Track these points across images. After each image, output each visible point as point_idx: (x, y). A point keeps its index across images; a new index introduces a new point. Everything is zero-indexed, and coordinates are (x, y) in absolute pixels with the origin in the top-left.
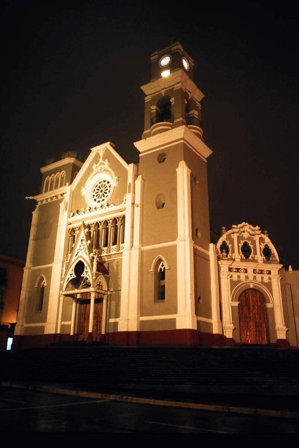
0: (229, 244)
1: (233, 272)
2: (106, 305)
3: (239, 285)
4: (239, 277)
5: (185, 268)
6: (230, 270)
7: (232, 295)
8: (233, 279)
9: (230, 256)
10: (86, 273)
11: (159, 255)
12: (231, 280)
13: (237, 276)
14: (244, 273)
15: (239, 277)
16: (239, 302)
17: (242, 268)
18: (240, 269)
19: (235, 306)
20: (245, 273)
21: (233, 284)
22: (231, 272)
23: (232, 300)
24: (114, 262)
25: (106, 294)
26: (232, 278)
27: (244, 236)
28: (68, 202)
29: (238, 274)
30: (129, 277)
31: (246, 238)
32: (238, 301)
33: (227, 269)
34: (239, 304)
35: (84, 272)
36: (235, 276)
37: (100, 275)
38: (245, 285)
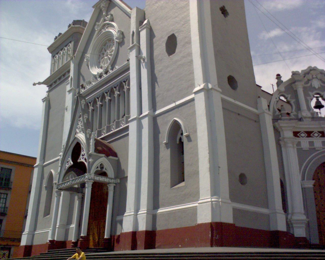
0: (290, 98)
1: (301, 138)
2: (40, 209)
3: (310, 159)
4: (311, 143)
5: (120, 74)
6: (296, 134)
7: (302, 171)
8: (302, 147)
9: (294, 115)
10: (82, 157)
11: (175, 119)
12: (298, 150)
13: (308, 143)
14: (320, 137)
15: (311, 143)
16: (314, 181)
17: (316, 130)
18: (312, 132)
19: (309, 188)
20: (321, 138)
21: (302, 154)
22: (298, 137)
23: (303, 179)
24: (102, 136)
25: (110, 183)
26: (301, 146)
27: (313, 86)
28: (73, 77)
29: (310, 139)
30: (45, 142)
31: (317, 87)
32: (313, 179)
33: (291, 135)
34: (314, 185)
35: (81, 157)
36: (305, 143)
37: (102, 157)
38: (312, 162)
